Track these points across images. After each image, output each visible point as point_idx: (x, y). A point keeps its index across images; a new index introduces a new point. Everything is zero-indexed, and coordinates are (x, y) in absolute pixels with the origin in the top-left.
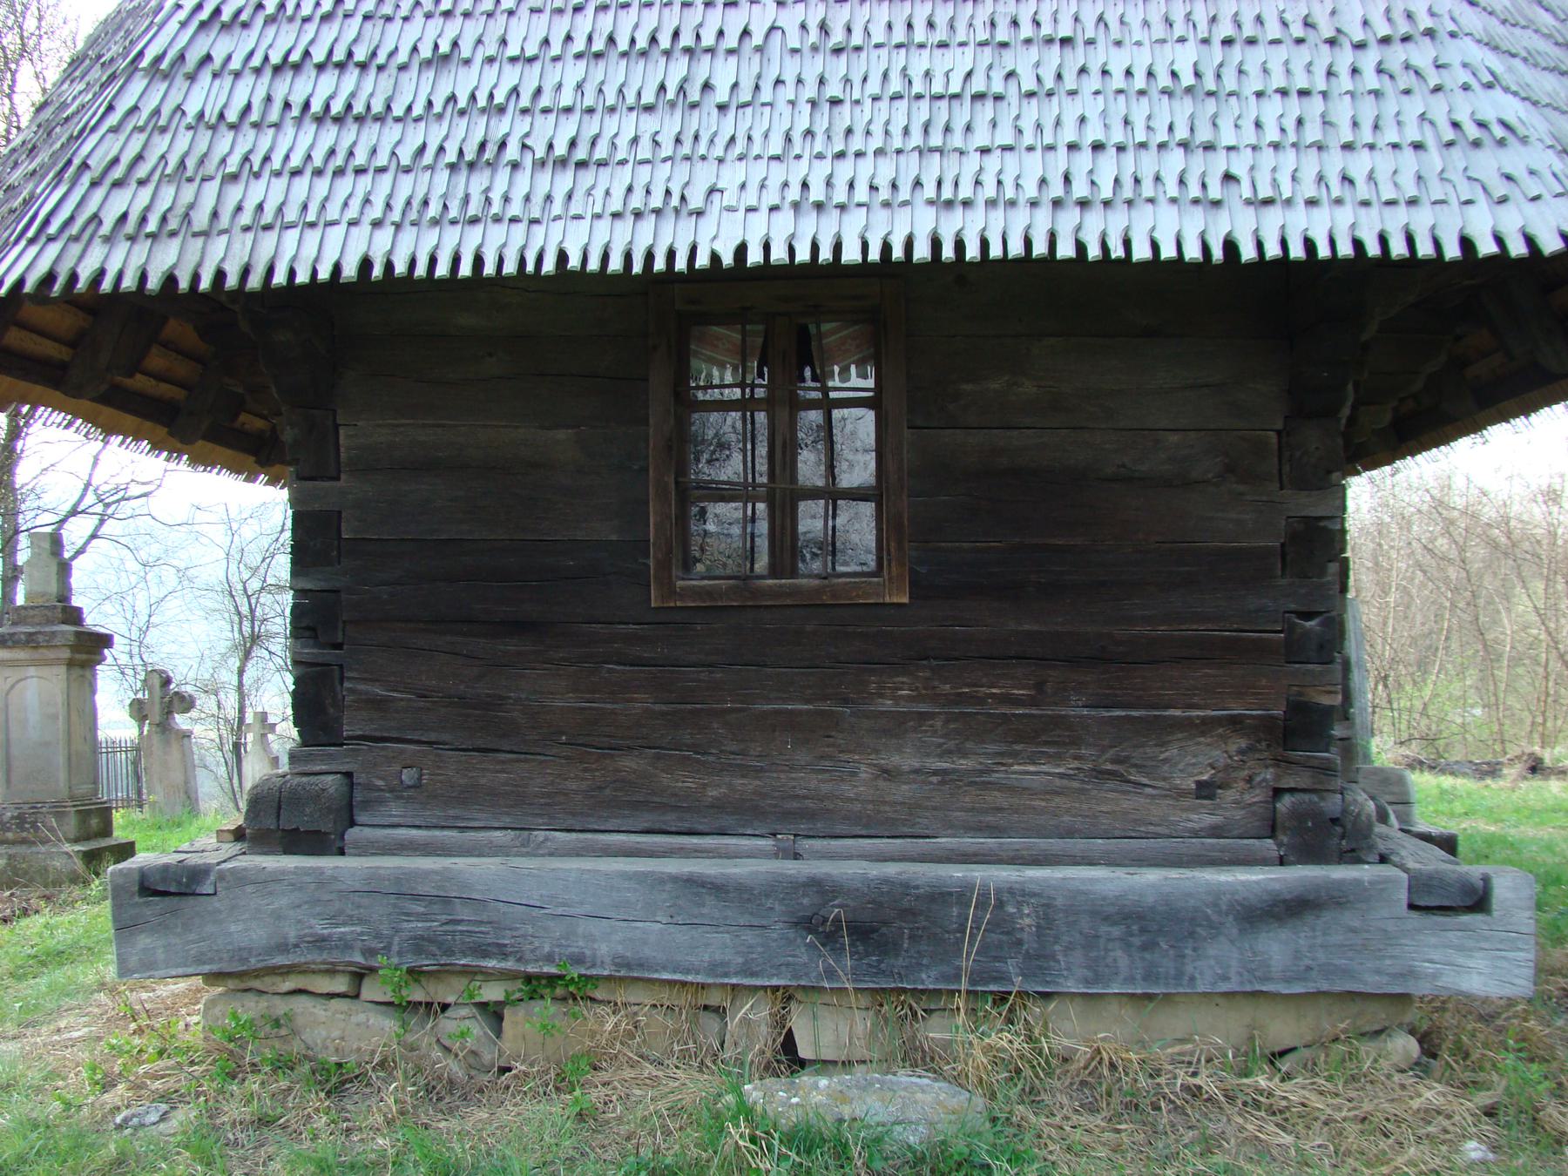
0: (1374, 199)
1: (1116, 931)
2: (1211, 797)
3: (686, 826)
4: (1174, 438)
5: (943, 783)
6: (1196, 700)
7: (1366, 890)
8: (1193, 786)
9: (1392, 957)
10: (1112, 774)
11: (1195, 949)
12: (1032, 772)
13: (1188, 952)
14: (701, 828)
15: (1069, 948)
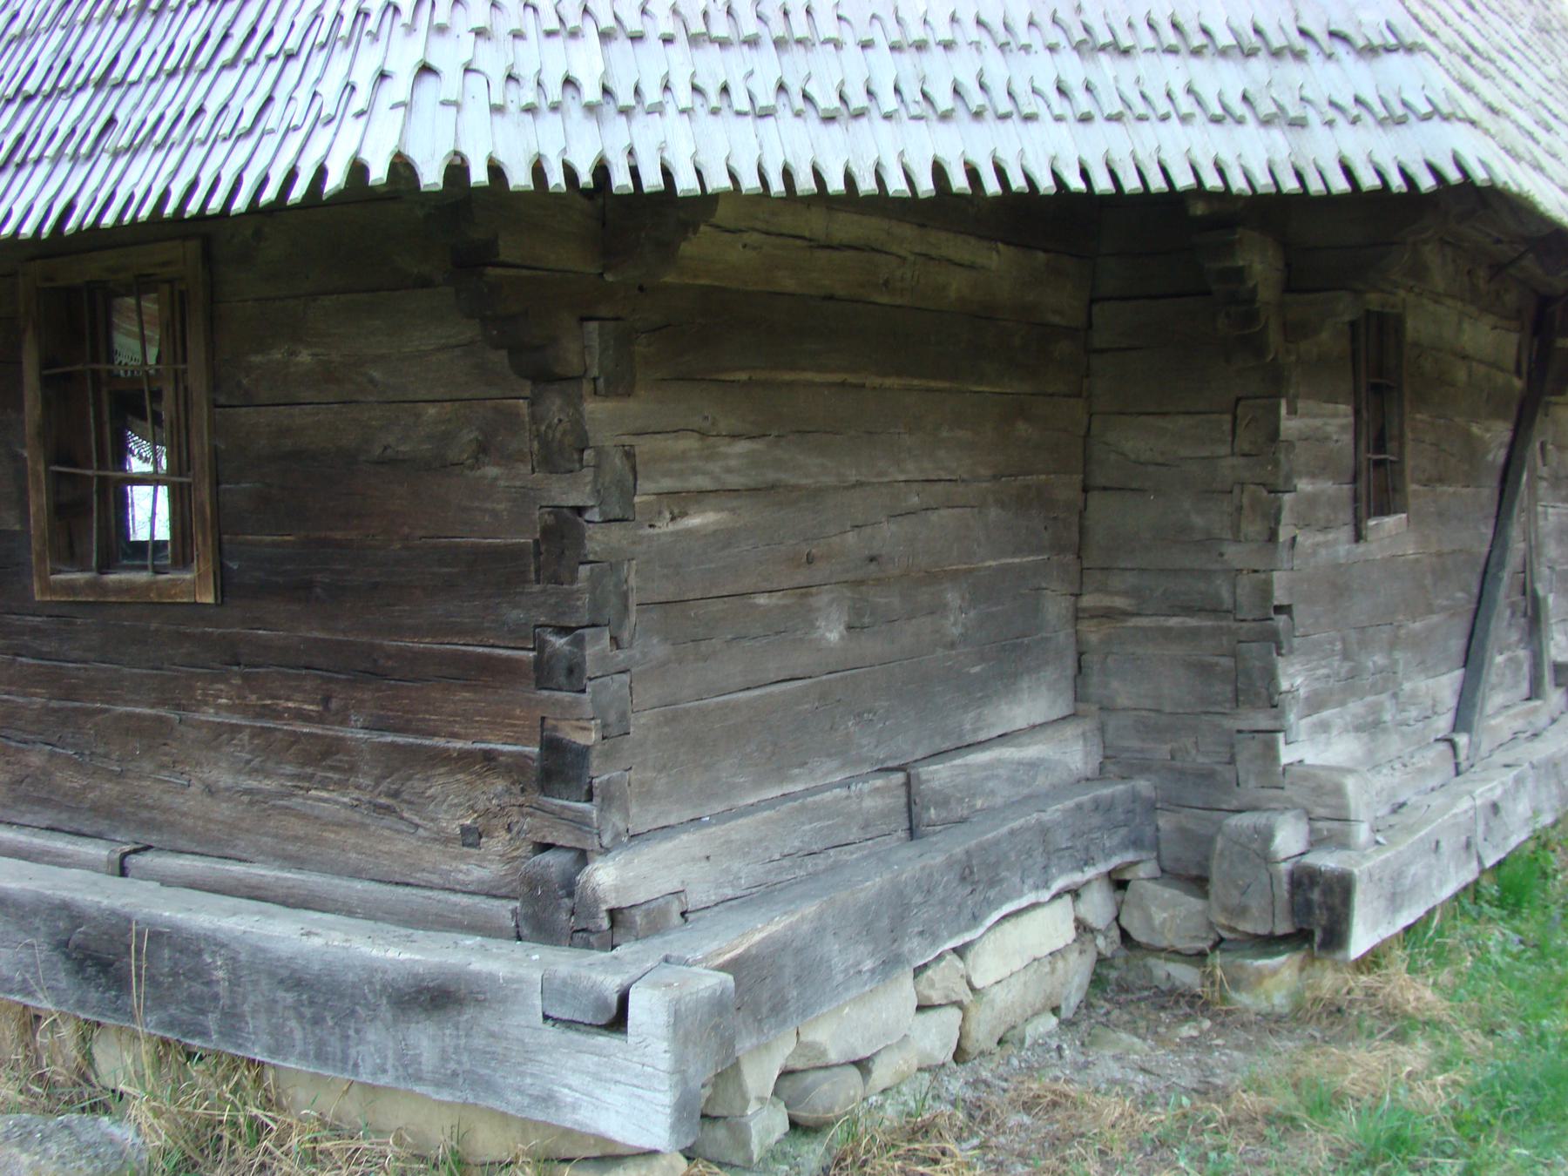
0: (1182, 47)
1: (290, 998)
2: (476, 845)
3: (75, 826)
4: (432, 410)
5: (251, 803)
6: (457, 728)
7: (500, 988)
8: (458, 831)
9: (532, 1075)
10: (389, 810)
11: (357, 1031)
12: (329, 801)
13: (351, 1032)
14: (85, 830)
15: (254, 1012)
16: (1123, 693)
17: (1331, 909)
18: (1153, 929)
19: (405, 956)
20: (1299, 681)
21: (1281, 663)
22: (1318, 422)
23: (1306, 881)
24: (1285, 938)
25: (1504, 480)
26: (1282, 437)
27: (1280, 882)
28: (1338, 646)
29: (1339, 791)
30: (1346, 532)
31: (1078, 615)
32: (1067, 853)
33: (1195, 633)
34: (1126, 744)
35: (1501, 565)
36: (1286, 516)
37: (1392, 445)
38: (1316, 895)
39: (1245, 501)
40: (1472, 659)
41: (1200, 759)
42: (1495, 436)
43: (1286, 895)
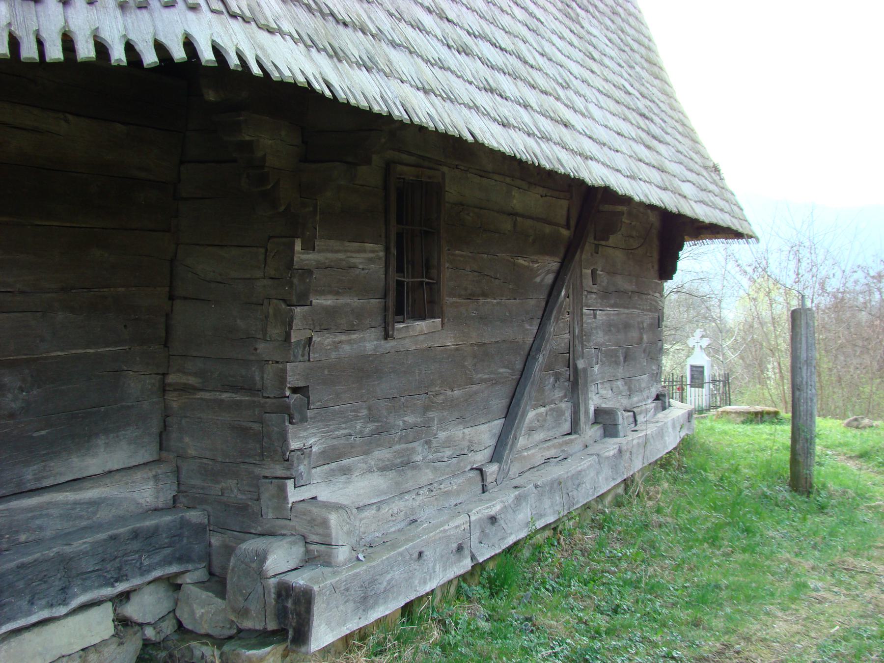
16: (192, 446)
17: (298, 614)
18: (195, 619)
19: (153, 522)
20: (312, 441)
21: (291, 429)
22: (341, 256)
23: (284, 593)
24: (274, 633)
25: (550, 295)
26: (296, 266)
27: (269, 592)
28: (365, 412)
29: (325, 523)
30: (379, 332)
31: (164, 389)
32: (93, 575)
33: (238, 405)
34: (193, 482)
35: (539, 350)
36: (297, 323)
37: (434, 272)
38: (289, 604)
39: (271, 311)
40: (511, 413)
41: (240, 496)
42: (545, 268)
43: (273, 602)
